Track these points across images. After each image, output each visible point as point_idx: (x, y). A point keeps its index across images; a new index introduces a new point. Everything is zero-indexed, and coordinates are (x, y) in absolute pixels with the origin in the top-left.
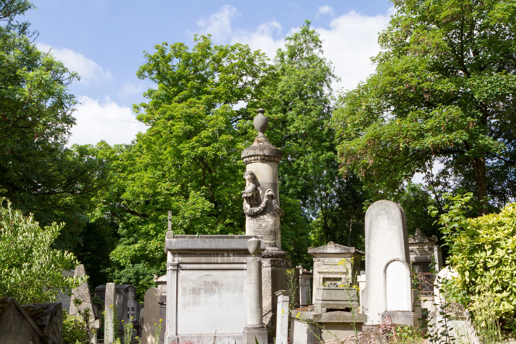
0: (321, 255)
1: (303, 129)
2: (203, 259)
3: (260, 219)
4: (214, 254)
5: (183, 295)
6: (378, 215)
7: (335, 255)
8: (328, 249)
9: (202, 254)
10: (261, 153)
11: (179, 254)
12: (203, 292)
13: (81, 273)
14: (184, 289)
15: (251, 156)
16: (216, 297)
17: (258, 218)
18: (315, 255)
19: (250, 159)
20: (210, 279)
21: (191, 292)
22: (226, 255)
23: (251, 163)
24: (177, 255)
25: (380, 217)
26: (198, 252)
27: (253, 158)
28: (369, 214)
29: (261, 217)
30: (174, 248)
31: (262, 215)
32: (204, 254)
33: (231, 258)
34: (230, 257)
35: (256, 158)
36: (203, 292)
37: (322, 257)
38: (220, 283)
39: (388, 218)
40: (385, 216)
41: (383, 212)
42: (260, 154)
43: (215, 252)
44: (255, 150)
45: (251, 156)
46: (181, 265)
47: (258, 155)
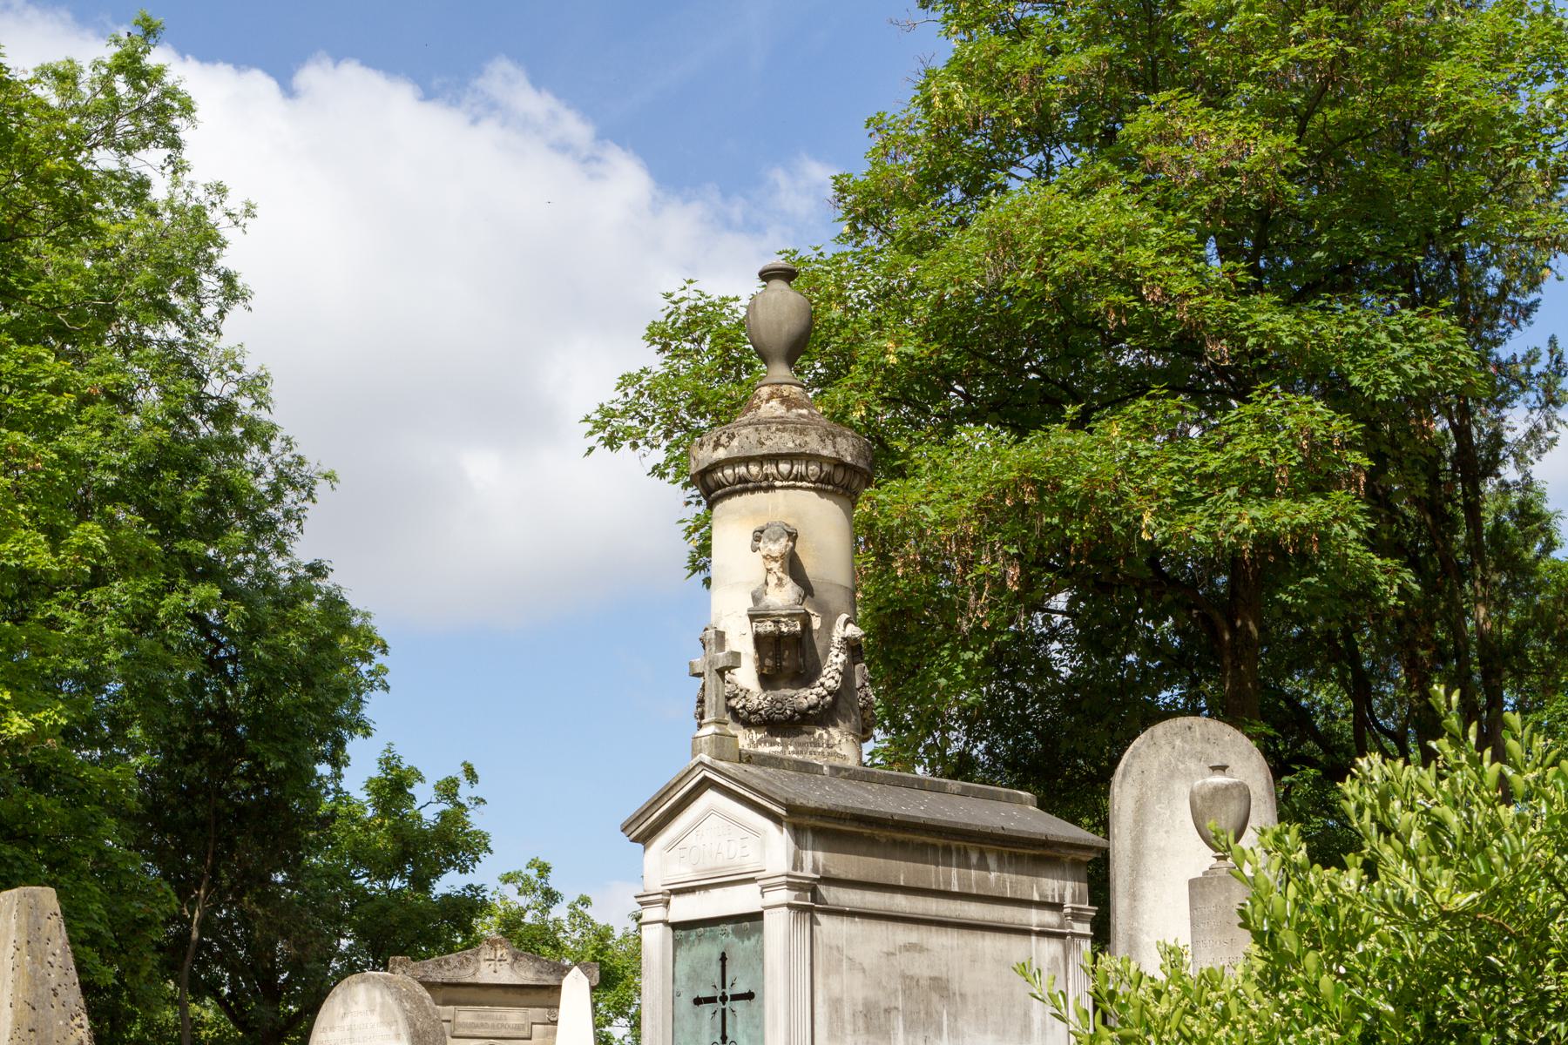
1: (111, 468)
2: (901, 870)
3: (816, 744)
4: (934, 846)
6: (1172, 776)
7: (511, 996)
8: (484, 965)
9: (894, 843)
10: (827, 452)
11: (819, 833)
12: (899, 1023)
13: (45, 932)
14: (835, 1004)
15: (775, 458)
17: (804, 738)
19: (770, 469)
20: (921, 967)
21: (861, 1023)
22: (974, 858)
23: (772, 488)
24: (810, 837)
26: (882, 834)
27: (784, 467)
28: (1135, 770)
29: (818, 732)
30: (812, 804)
31: (824, 726)
32: (903, 845)
33: (993, 875)
34: (987, 869)
35: (799, 468)
36: (899, 1023)
38: (955, 986)
42: (825, 453)
43: (940, 842)
44: (802, 432)
46: (822, 889)
47: (810, 458)
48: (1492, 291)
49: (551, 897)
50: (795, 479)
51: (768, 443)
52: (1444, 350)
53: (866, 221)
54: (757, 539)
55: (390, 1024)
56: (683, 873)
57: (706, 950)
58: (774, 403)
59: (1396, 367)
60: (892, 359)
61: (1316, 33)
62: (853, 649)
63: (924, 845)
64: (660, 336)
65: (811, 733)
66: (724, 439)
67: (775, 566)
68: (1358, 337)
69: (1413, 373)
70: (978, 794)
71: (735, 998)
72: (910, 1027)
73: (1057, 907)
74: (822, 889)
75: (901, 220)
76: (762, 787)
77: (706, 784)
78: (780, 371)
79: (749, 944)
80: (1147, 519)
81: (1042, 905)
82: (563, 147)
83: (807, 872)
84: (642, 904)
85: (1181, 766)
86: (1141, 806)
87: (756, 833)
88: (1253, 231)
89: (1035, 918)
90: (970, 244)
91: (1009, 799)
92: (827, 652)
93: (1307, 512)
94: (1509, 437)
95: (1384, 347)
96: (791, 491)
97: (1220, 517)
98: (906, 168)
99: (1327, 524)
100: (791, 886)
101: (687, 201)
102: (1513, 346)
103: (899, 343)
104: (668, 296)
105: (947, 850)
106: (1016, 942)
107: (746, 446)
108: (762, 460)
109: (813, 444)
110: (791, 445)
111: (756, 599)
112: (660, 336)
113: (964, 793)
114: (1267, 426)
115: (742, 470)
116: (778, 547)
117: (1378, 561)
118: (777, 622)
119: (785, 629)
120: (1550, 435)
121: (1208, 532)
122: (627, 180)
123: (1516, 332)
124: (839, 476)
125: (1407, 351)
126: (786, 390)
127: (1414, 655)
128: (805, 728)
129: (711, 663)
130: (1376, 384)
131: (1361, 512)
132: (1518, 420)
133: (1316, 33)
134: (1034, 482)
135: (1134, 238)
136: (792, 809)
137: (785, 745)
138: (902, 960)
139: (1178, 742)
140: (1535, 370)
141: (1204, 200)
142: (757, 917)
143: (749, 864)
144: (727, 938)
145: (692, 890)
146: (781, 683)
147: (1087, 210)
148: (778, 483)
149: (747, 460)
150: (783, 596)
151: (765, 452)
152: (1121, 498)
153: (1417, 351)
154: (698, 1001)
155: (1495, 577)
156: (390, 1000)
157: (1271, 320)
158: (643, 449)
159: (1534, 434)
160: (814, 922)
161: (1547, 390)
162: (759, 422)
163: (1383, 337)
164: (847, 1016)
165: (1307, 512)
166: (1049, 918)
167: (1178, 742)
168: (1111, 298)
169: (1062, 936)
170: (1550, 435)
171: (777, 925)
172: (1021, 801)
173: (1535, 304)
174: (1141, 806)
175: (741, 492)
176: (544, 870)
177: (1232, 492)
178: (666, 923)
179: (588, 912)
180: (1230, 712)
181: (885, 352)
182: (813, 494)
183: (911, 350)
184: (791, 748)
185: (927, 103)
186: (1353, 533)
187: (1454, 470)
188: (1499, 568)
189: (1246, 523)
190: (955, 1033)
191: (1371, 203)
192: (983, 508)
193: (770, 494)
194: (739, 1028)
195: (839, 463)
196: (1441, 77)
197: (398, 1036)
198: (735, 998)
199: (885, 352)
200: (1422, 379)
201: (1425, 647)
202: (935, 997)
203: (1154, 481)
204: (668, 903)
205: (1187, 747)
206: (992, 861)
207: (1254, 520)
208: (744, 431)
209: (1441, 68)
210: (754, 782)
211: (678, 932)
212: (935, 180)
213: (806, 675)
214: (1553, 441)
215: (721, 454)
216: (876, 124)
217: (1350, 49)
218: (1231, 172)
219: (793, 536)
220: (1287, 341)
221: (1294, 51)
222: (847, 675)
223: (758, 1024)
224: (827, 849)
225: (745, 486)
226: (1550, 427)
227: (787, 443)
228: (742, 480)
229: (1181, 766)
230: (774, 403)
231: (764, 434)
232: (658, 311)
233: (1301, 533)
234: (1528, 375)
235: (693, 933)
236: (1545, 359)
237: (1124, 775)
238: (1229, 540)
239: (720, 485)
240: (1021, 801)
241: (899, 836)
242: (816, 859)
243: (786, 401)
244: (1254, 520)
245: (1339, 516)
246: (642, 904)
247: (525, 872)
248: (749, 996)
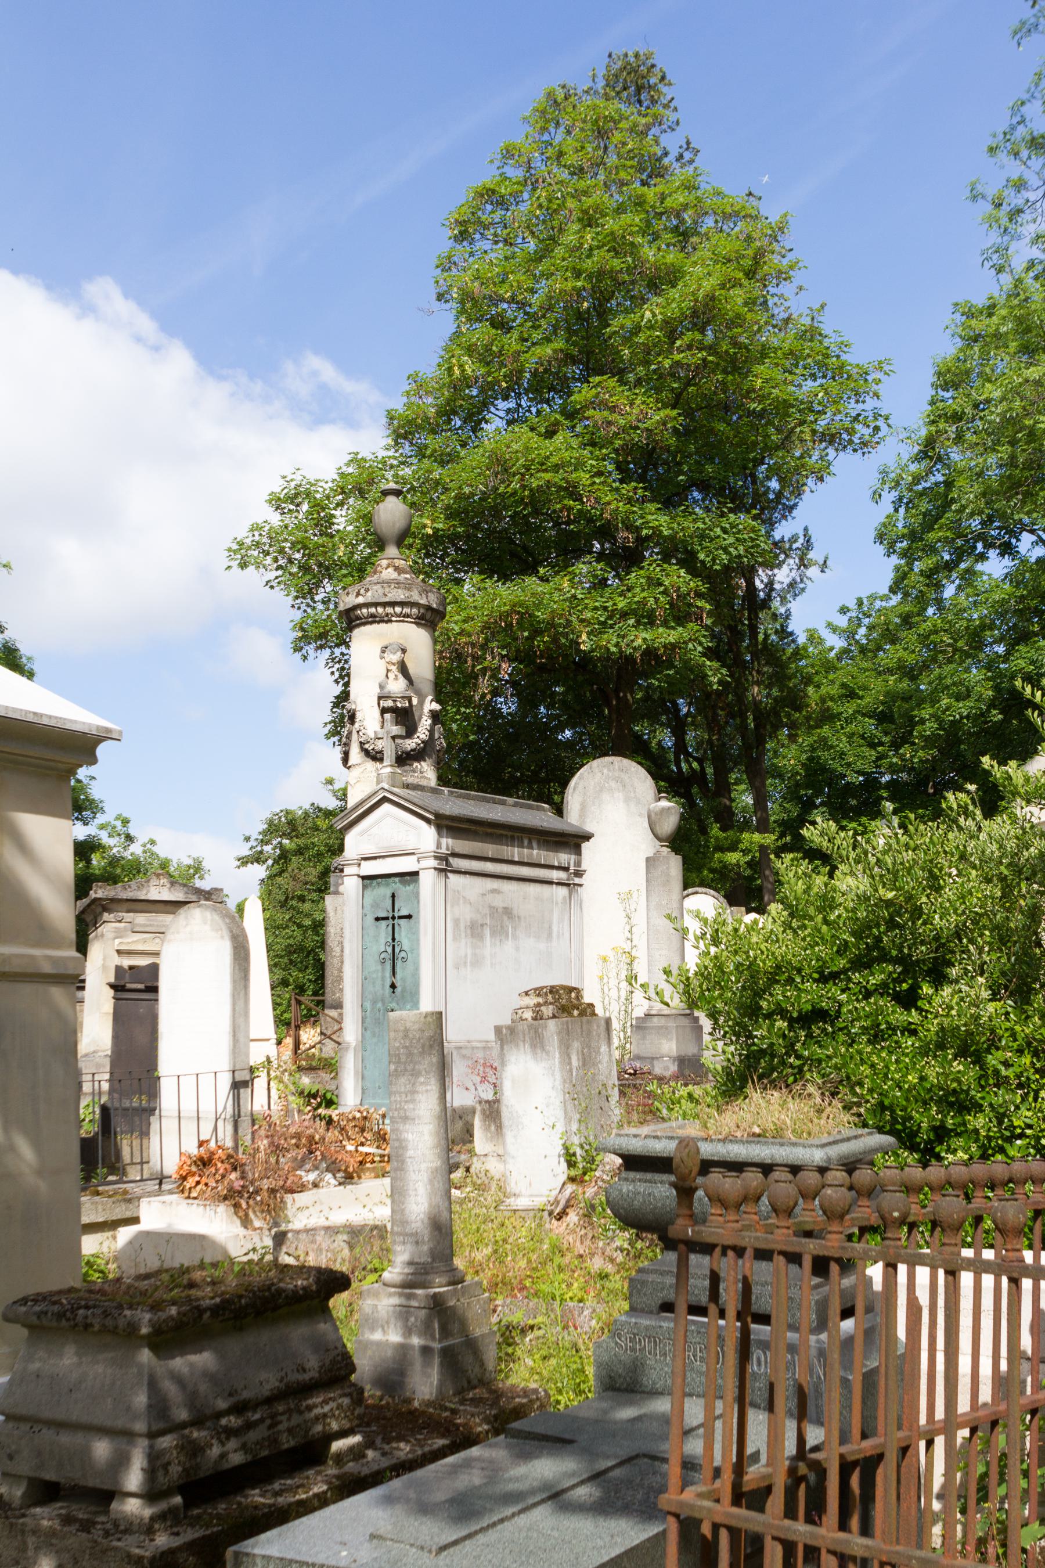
0: (126, 905)
2: (490, 849)
3: (414, 771)
5: (455, 939)
6: (601, 790)
7: (169, 908)
8: (152, 889)
10: (423, 601)
12: (487, 932)
14: (457, 922)
15: (393, 604)
16: (509, 946)
17: (407, 768)
18: (111, 906)
19: (389, 610)
20: (498, 902)
22: (526, 842)
23: (391, 621)
25: (606, 796)
26: (480, 829)
27: (398, 610)
29: (416, 764)
31: (419, 761)
32: (491, 835)
33: (535, 852)
35: (407, 610)
36: (487, 932)
37: (128, 911)
38: (515, 912)
39: (627, 800)
40: (620, 795)
41: (613, 784)
43: (510, 834)
44: (409, 589)
45: (393, 604)
46: (451, 859)
48: (772, 496)
49: (129, 838)
52: (753, 540)
53: (405, 438)
54: (383, 652)
56: (371, 850)
57: (383, 892)
58: (390, 570)
59: (725, 550)
60: (430, 531)
61: (690, 347)
62: (435, 716)
63: (501, 835)
64: (277, 502)
66: (362, 591)
67: (394, 668)
68: (704, 530)
69: (734, 552)
70: (522, 806)
71: (400, 917)
72: (493, 934)
73: (566, 869)
74: (451, 859)
75: (433, 443)
76: (420, 803)
77: (384, 800)
78: (392, 551)
79: (410, 888)
80: (584, 637)
81: (560, 868)
82: (139, 339)
83: (444, 850)
87: (415, 828)
88: (644, 464)
89: (556, 875)
90: (474, 458)
91: (538, 808)
92: (420, 718)
93: (672, 636)
94: (777, 586)
95: (719, 537)
97: (623, 637)
98: (430, 405)
99: (684, 642)
100: (436, 858)
101: (221, 378)
102: (783, 530)
103: (433, 521)
104: (284, 477)
105: (513, 838)
106: (546, 888)
108: (385, 605)
109: (415, 597)
111: (382, 687)
112: (277, 502)
113: (515, 805)
114: (654, 582)
115: (373, 610)
116: (396, 657)
117: (708, 663)
120: (802, 586)
121: (617, 645)
122: (180, 362)
123: (784, 522)
124: (429, 615)
125: (731, 540)
126: (397, 562)
127: (715, 715)
129: (388, 733)
130: (714, 560)
131: (704, 636)
132: (783, 576)
133: (690, 347)
134: (519, 613)
135: (579, 465)
136: (438, 816)
138: (489, 898)
140: (795, 546)
141: (618, 443)
142: (416, 874)
143: (410, 846)
144: (396, 885)
145: (375, 858)
147: (549, 446)
149: (376, 605)
150: (397, 686)
152: (569, 623)
153: (738, 540)
154: (377, 919)
155: (765, 669)
156: (217, 917)
157: (658, 520)
158: (262, 570)
159: (792, 585)
160: (446, 877)
161: (801, 559)
162: (383, 582)
163: (718, 531)
164: (462, 928)
165: (672, 636)
166: (562, 875)
167: (605, 771)
168: (565, 502)
169: (568, 885)
170: (802, 586)
171: (428, 880)
172: (544, 809)
173: (795, 505)
175: (371, 623)
176: (126, 822)
177: (631, 622)
179: (155, 849)
180: (618, 750)
181: (425, 526)
183: (440, 526)
185: (450, 370)
186: (700, 649)
187: (743, 605)
188: (767, 663)
189: (640, 641)
190: (515, 937)
191: (712, 449)
192: (486, 627)
194: (403, 934)
195: (429, 608)
196: (761, 374)
197: (222, 937)
198: (400, 917)
199: (425, 526)
200: (739, 556)
201: (722, 709)
202: (505, 918)
203: (588, 615)
206: (535, 845)
207: (644, 639)
208: (375, 587)
209: (759, 369)
210: (416, 800)
212: (447, 412)
213: (411, 731)
214: (803, 590)
215: (361, 600)
216: (413, 378)
217: (710, 358)
218: (637, 428)
219: (404, 651)
220: (666, 533)
221: (677, 357)
222: (431, 731)
223: (415, 933)
224: (453, 838)
225: (374, 619)
226: (802, 581)
227: (400, 595)
228: (373, 616)
230: (390, 570)
232: (277, 486)
233: (672, 647)
234: (790, 549)
235: (375, 882)
236: (801, 540)
238: (629, 651)
239: (358, 618)
240: (544, 809)
241: (489, 830)
242: (448, 843)
243: (396, 569)
244: (644, 639)
245: (690, 639)
247: (113, 823)
248: (409, 917)
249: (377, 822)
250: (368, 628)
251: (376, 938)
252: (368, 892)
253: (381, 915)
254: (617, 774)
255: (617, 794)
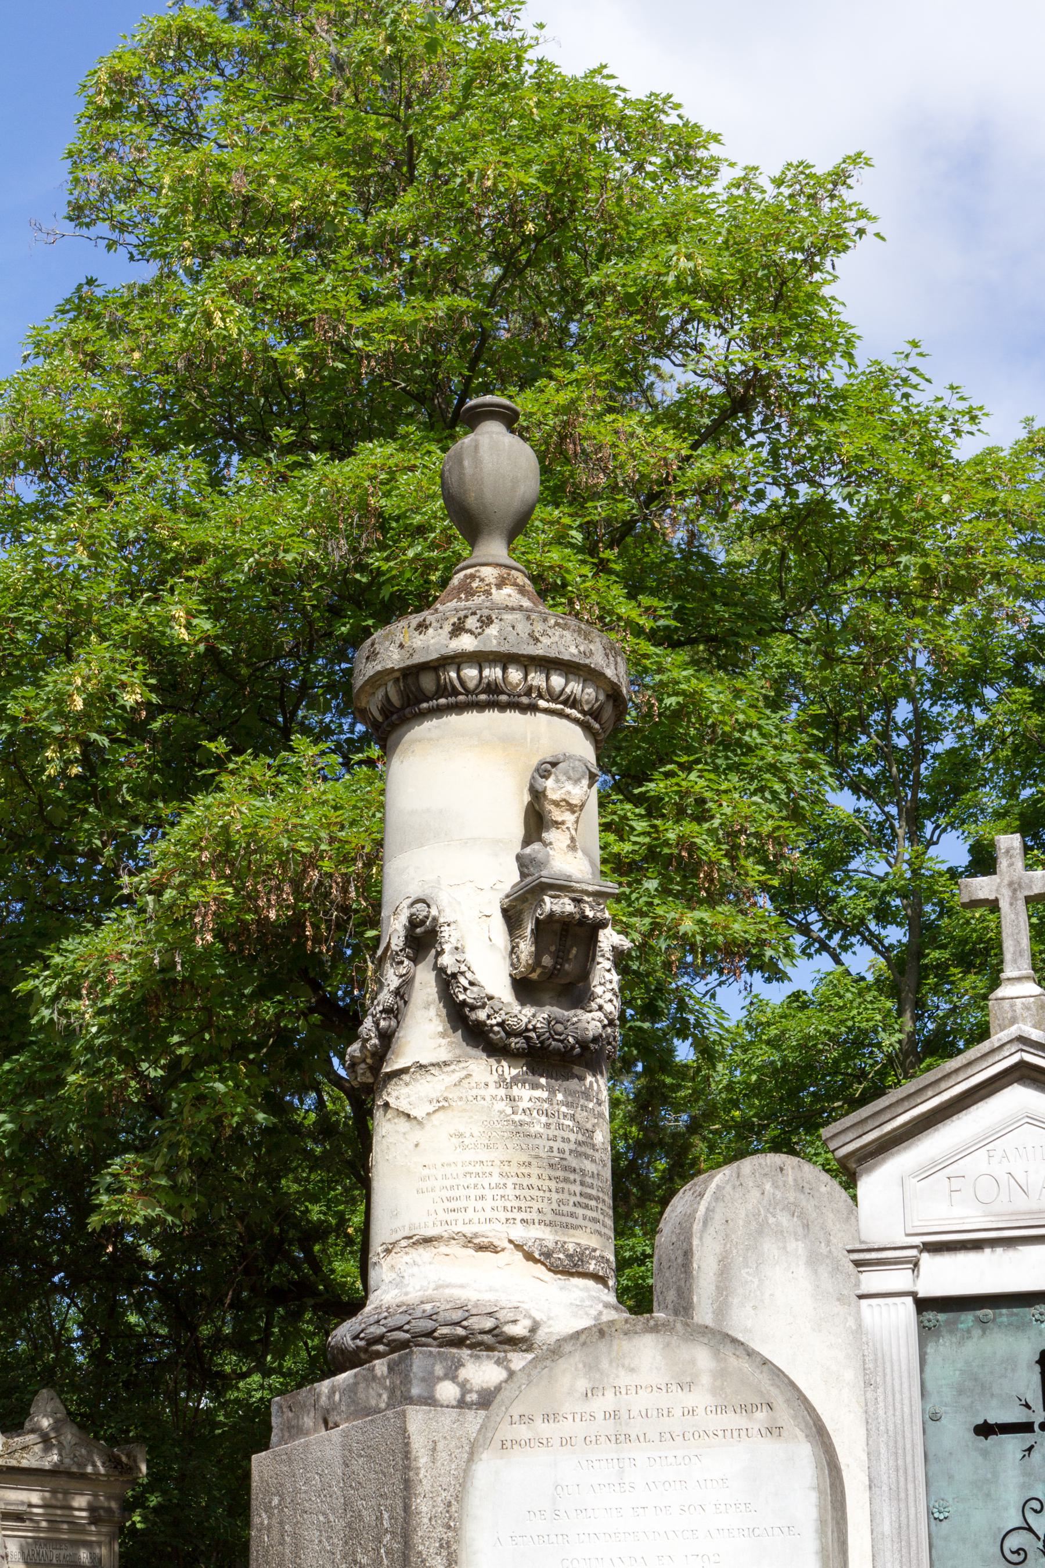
6: (760, 1232)
15: (548, 664)
17: (573, 1084)
19: (537, 679)
23: (533, 708)
25: (769, 1246)
27: (557, 681)
28: (718, 1218)
29: (589, 1079)
35: (575, 687)
39: (813, 1260)
40: (798, 1247)
41: (784, 1219)
50: (565, 703)
51: (545, 640)
55: (747, 1409)
58: (508, 590)
65: (582, 1079)
66: (472, 623)
84: (858, 1264)
85: (772, 1220)
86: (725, 1270)
96: (555, 719)
107: (512, 638)
110: (573, 650)
115: (493, 673)
118: (577, 901)
119: (590, 914)
128: (577, 1070)
137: (552, 1092)
139: (768, 1186)
145: (977, 1245)
146: (546, 997)
148: (542, 704)
149: (505, 660)
151: (540, 652)
154: (985, 1430)
167: (768, 1186)
174: (725, 1270)
175: (481, 707)
178: (913, 1294)
182: (578, 730)
184: (560, 1097)
193: (528, 717)
204: (916, 1265)
205: (779, 1195)
208: (508, 617)
211: (930, 1315)
215: (466, 643)
225: (494, 698)
228: (492, 688)
229: (772, 1220)
231: (539, 627)
235: (968, 1318)
237: (705, 1223)
239: (444, 690)
246: (858, 1264)
249: (985, 1141)
250: (471, 719)
251: (985, 1488)
252: (942, 1349)
253: (995, 1417)
254: (791, 1196)
255: (792, 1245)
